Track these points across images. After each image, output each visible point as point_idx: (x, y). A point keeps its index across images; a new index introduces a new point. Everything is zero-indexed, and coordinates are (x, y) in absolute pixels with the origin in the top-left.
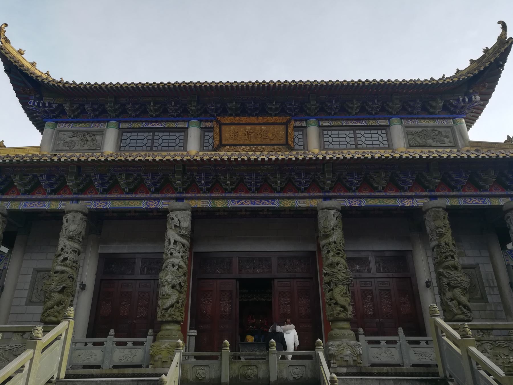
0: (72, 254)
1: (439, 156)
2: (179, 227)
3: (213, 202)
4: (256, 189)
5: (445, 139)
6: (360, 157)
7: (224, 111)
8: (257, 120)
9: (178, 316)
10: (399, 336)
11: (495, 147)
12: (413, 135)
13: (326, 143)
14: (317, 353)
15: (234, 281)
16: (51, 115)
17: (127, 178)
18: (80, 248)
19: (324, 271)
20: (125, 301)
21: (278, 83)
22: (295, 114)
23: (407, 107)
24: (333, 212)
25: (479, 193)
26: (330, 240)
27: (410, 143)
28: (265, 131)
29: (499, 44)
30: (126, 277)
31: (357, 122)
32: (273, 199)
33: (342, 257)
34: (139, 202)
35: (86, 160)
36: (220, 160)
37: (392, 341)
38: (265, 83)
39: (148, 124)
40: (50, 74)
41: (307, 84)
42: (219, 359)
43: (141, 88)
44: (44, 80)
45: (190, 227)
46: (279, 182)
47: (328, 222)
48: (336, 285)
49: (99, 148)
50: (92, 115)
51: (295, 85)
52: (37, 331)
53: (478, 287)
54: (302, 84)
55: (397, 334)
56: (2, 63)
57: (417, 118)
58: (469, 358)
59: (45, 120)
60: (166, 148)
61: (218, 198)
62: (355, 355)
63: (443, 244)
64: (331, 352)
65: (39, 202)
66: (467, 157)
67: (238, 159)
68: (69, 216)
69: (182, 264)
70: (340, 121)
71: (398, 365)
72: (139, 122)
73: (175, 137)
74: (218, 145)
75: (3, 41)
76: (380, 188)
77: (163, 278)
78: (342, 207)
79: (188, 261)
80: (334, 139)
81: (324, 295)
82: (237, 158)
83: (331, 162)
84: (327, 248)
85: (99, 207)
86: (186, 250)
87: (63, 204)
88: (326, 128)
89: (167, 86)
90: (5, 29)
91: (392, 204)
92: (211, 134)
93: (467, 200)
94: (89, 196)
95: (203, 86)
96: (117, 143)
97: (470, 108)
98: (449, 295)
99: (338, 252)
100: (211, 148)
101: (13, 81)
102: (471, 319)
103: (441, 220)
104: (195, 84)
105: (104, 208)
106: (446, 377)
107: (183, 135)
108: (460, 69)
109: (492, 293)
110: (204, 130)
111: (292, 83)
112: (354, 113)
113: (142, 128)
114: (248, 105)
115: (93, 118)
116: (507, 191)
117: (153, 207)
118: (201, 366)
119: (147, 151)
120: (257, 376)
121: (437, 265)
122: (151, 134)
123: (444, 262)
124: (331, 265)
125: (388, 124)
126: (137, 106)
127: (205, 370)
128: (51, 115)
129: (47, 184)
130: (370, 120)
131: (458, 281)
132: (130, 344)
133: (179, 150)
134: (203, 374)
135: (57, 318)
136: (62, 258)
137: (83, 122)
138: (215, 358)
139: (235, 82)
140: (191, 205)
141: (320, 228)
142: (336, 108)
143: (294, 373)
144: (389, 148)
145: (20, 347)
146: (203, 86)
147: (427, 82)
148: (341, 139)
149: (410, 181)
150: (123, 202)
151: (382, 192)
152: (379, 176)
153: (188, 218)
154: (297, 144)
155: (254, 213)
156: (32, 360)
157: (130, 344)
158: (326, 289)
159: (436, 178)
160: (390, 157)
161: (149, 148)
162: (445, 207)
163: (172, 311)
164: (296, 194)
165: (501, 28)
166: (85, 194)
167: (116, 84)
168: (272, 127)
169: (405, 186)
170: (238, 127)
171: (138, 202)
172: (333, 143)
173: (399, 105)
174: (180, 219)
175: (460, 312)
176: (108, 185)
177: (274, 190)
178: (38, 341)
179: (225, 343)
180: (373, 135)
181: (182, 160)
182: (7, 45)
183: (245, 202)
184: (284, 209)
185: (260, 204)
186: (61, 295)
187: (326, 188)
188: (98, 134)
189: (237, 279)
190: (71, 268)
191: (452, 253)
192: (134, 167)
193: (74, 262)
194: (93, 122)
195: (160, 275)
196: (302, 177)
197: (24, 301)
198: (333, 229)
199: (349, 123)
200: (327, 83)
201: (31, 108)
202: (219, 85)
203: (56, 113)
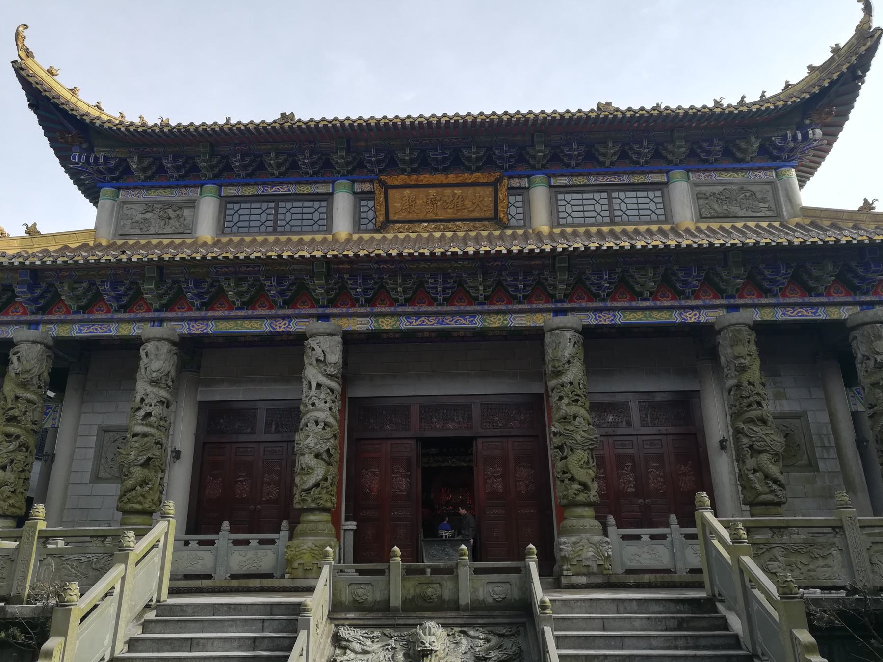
0: (158, 407)
1: (742, 242)
2: (324, 362)
3: (377, 322)
4: (445, 299)
5: (762, 205)
6: (612, 247)
7: (391, 164)
8: (446, 178)
9: (326, 501)
10: (670, 528)
11: (843, 218)
12: (707, 198)
13: (561, 215)
14: (527, 565)
16: (108, 177)
17: (238, 285)
19: (553, 429)
20: (242, 476)
21: (480, 117)
22: (511, 167)
23: (698, 151)
24: (568, 334)
25: (807, 299)
26: (563, 379)
27: (701, 212)
28: (461, 197)
29: (857, 39)
30: (243, 438)
31: (614, 178)
32: (473, 314)
33: (581, 406)
34: (259, 323)
35: (172, 260)
36: (385, 255)
37: (658, 535)
38: (459, 116)
39: (266, 188)
40: (102, 106)
41: (529, 118)
42: (386, 574)
43: (253, 131)
44: (94, 121)
45: (341, 361)
46: (481, 288)
47: (560, 352)
48: (572, 450)
49: (188, 230)
50: (176, 175)
51: (509, 120)
52: (127, 539)
53: (805, 449)
54: (520, 118)
55: (667, 525)
56: (24, 92)
57: (716, 170)
58: (741, 571)
59: (99, 185)
60: (299, 229)
61: (384, 315)
62: (600, 558)
63: (745, 384)
64: (563, 554)
65: (102, 325)
66: (787, 244)
67: (415, 254)
68: (150, 347)
69: (331, 420)
70: (585, 177)
71: (668, 571)
72: (252, 185)
73: (312, 210)
74: (384, 222)
75: (23, 55)
76: (646, 294)
77: (302, 443)
80: (575, 209)
82: (412, 251)
84: (559, 392)
85: (196, 332)
86: (336, 397)
88: (561, 189)
89: (296, 126)
90: (24, 34)
91: (666, 319)
92: (371, 203)
93: (788, 312)
94: (179, 314)
95: (356, 124)
97: (806, 150)
98: (751, 463)
100: (371, 226)
102: (784, 500)
103: (743, 345)
104: (342, 122)
105: (203, 333)
106: (714, 595)
107: (326, 205)
108: (792, 83)
109: (826, 456)
110: (359, 196)
111: (504, 116)
112: (608, 164)
113: (258, 195)
114: (431, 153)
115: (177, 180)
116: (856, 295)
117: (281, 329)
118: (360, 584)
119: (269, 234)
120: (440, 597)
121: (736, 416)
122: (272, 205)
123: (746, 411)
124: (565, 419)
125: (666, 181)
126: (248, 160)
127: (365, 589)
128: (108, 177)
129: (113, 297)
130: (635, 175)
131: (765, 441)
132: (254, 543)
133: (319, 232)
134: (364, 594)
135: (142, 504)
136: (142, 413)
137: (161, 187)
138: (381, 572)
139: (409, 117)
140: (341, 326)
142: (579, 155)
143: (494, 592)
144: (666, 222)
145: (101, 557)
146: (356, 124)
147: (732, 109)
148: (586, 208)
149: (695, 283)
150: (232, 322)
152: (645, 275)
153: (338, 348)
154: (513, 217)
155: (444, 336)
156: (123, 579)
157: (254, 543)
158: (557, 456)
159: (737, 277)
161: (270, 229)
162: (751, 323)
163: (316, 492)
164: (510, 307)
165: (863, 10)
167: (212, 125)
168: (470, 191)
169: (687, 290)
171: (256, 323)
172: (573, 215)
173: (684, 149)
174: (324, 349)
175: (767, 490)
176: (208, 296)
177: (473, 300)
178: (130, 552)
179: (394, 551)
180: (640, 200)
181: (324, 256)
182: (29, 62)
183: (428, 320)
185: (451, 323)
186: (146, 471)
187: (558, 295)
189: (418, 439)
190: (157, 428)
191: (757, 398)
192: (248, 267)
193: (161, 419)
194: (177, 187)
196: (518, 278)
197: (87, 476)
198: (569, 362)
199: (600, 180)
200: (562, 115)
201: (75, 166)
202: (381, 123)
203: (117, 173)
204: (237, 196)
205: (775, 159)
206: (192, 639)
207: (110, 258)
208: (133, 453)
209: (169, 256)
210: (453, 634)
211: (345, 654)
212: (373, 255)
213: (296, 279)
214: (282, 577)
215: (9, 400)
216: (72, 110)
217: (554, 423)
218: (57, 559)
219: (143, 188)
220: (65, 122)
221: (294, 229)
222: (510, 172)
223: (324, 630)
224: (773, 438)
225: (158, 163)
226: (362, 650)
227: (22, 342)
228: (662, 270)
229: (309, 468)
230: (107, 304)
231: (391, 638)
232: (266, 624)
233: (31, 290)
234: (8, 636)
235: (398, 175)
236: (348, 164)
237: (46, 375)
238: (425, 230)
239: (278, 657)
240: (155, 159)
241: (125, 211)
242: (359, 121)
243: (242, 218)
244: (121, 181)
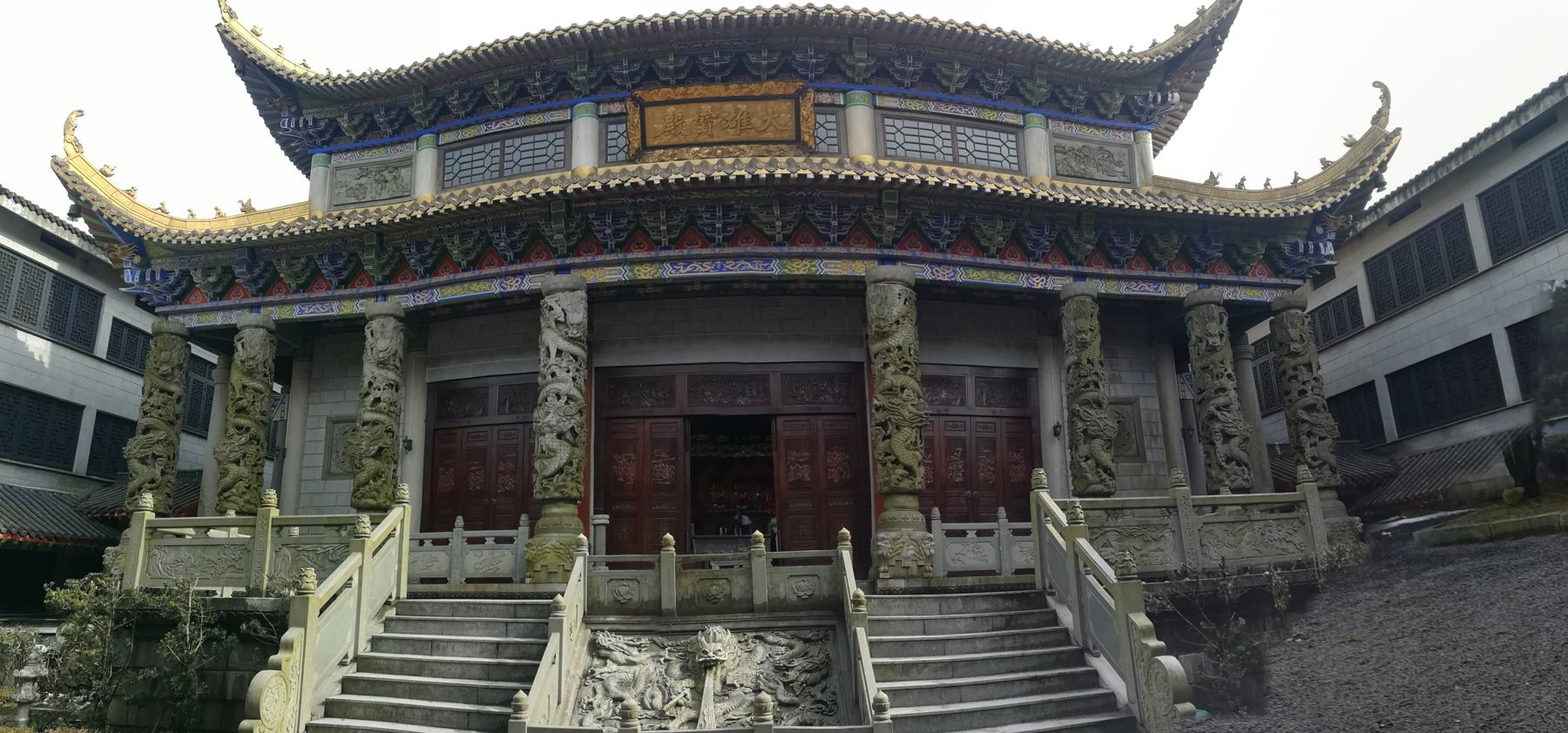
2: (565, 323)
3: (631, 270)
4: (725, 239)
5: (1117, 169)
7: (650, 77)
8: (727, 90)
9: (572, 489)
13: (890, 145)
15: (680, 421)
16: (319, 142)
17: (462, 242)
18: (398, 379)
19: (876, 402)
20: (475, 465)
21: (775, 11)
22: (818, 78)
25: (1151, 273)
32: (767, 258)
33: (911, 376)
36: (644, 183)
40: (307, 63)
42: (656, 567)
45: (586, 321)
46: (779, 223)
48: (898, 428)
49: (406, 193)
50: (389, 131)
56: (230, 58)
59: (310, 151)
60: (530, 169)
61: (641, 262)
63: (1085, 362)
68: (374, 324)
69: (575, 392)
75: (226, 16)
76: (993, 250)
78: (917, 280)
79: (586, 386)
81: (874, 447)
83: (897, 186)
85: (422, 303)
87: (362, 305)
88: (890, 113)
92: (622, 128)
94: (403, 286)
96: (438, 175)
99: (905, 365)
100: (622, 156)
101: (251, 88)
110: (606, 120)
113: (481, 136)
114: (704, 60)
117: (513, 289)
119: (494, 180)
121: (1072, 397)
122: (498, 145)
123: (1083, 392)
124: (890, 391)
126: (467, 96)
129: (331, 271)
132: (490, 541)
133: (555, 169)
134: (628, 593)
136: (371, 398)
137: (374, 146)
138: (649, 566)
140: (585, 279)
141: (869, 319)
143: (799, 588)
151: (995, 257)
154: (823, 141)
155: (722, 287)
157: (490, 541)
159: (1088, 242)
160: (1014, 193)
161: (496, 175)
162: (1096, 295)
164: (820, 249)
166: (396, 282)
168: (760, 106)
170: (683, 107)
174: (565, 308)
177: (768, 240)
181: (563, 192)
182: (233, 24)
184: (795, 279)
185: (733, 269)
186: (378, 462)
187: (884, 239)
188: (402, 167)
189: (685, 417)
190: (387, 414)
192: (473, 219)
194: (392, 144)
195: (535, 414)
198: (897, 322)
203: (328, 136)
204: (456, 142)
205: (1135, 120)
206: (432, 641)
207: (326, 226)
208: (364, 443)
209: (389, 218)
210: (746, 641)
211: (605, 665)
212: (627, 184)
213: (529, 226)
214: (523, 581)
215: (237, 390)
216: (279, 70)
217: (877, 395)
218: (293, 550)
219: (356, 149)
220: (265, 78)
221: (524, 170)
222: (818, 84)
223: (578, 636)
224: (1105, 421)
225: (369, 119)
226: (627, 660)
227: (245, 327)
228: (1012, 224)
229: (550, 450)
230: (326, 281)
231: (664, 648)
232: (511, 627)
233: (250, 270)
234: (249, 628)
235: (659, 89)
236: (591, 81)
237: (270, 361)
238: (696, 155)
239: (526, 665)
240: (366, 115)
241: (339, 178)
242: (605, 25)
243: (464, 167)
244: (332, 145)
